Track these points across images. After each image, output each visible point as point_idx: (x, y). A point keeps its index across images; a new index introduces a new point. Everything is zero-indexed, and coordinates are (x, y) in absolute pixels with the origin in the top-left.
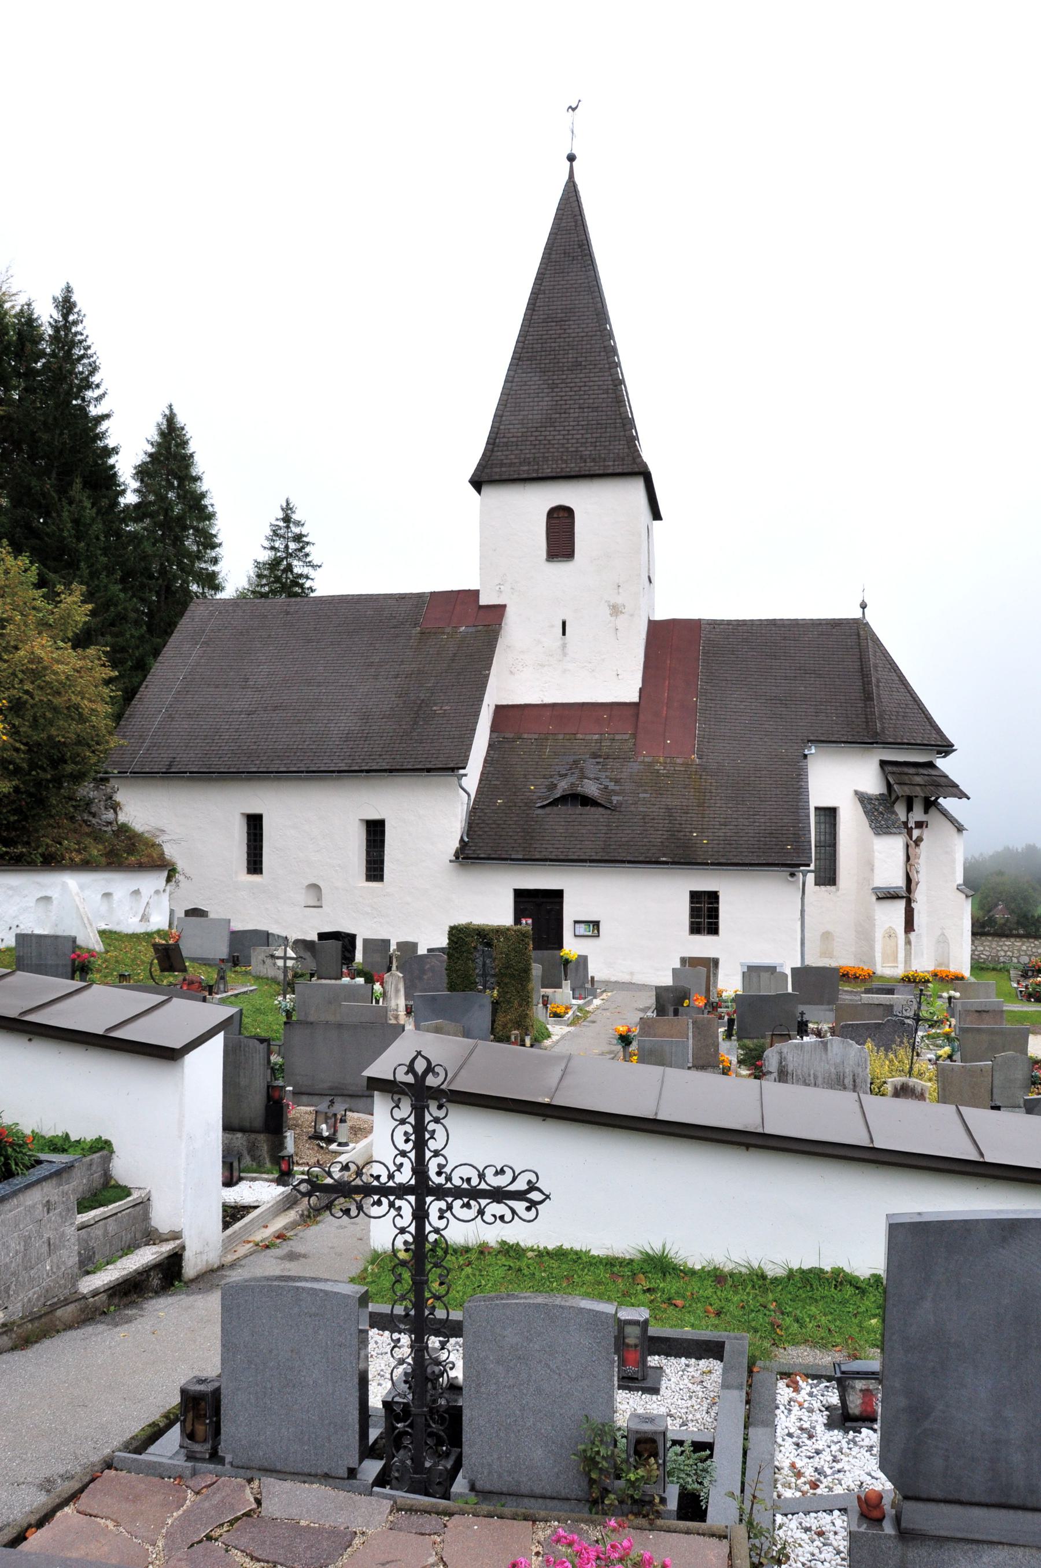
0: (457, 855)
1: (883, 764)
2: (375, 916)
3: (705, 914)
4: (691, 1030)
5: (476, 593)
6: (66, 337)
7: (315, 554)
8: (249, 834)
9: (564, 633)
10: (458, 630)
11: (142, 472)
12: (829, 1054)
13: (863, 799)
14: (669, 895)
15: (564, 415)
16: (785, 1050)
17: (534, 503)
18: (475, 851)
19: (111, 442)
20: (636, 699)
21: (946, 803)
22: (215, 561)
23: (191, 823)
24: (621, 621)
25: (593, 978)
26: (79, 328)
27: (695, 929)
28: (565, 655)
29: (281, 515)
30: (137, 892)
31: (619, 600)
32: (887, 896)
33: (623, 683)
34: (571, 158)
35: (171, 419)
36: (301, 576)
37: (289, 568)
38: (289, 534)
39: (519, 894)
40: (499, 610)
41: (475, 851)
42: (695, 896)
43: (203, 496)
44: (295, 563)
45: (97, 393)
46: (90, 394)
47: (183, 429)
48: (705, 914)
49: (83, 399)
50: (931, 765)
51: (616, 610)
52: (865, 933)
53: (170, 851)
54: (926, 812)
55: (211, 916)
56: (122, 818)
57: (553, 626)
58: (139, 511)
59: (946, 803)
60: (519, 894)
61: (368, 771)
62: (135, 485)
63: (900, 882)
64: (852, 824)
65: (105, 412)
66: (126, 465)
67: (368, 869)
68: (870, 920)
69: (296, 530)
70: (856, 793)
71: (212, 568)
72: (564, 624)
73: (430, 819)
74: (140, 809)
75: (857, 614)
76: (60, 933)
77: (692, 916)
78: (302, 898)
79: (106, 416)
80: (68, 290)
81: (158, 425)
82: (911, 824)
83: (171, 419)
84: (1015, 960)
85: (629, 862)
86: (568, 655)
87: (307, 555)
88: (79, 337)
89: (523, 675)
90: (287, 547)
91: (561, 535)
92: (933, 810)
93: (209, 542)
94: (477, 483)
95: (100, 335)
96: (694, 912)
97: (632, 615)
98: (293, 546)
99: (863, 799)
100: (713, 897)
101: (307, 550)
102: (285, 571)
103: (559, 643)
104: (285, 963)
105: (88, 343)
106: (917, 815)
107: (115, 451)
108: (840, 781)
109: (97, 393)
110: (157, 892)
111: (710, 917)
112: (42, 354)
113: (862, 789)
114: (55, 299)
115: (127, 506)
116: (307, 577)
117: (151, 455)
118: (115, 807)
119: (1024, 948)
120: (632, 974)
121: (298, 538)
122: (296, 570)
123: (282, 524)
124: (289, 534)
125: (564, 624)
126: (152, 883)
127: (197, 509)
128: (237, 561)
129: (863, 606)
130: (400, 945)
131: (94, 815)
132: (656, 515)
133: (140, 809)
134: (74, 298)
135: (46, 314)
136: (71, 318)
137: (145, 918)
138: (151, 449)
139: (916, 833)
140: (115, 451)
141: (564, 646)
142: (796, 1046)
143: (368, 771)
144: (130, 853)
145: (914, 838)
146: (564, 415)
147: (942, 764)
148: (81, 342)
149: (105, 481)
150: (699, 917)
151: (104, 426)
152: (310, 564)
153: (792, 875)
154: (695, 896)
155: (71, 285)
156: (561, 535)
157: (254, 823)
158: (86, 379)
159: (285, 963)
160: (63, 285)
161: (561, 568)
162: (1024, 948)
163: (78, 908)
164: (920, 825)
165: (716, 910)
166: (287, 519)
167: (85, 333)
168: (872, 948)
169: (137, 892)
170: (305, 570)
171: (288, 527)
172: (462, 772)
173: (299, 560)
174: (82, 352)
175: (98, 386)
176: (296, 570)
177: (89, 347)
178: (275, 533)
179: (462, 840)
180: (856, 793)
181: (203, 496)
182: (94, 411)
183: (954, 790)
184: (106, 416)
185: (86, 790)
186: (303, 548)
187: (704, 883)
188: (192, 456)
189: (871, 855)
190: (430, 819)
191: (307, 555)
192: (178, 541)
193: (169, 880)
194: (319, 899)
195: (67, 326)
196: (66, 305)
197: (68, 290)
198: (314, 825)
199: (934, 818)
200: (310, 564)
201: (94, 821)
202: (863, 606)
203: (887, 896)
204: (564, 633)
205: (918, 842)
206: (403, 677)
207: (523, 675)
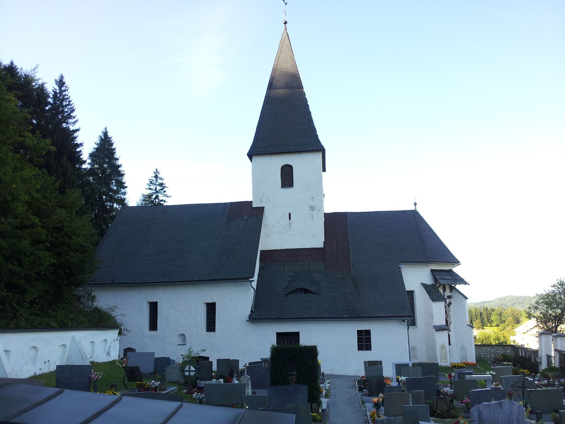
0: (250, 317)
1: (432, 271)
2: (218, 348)
3: (364, 340)
4: (411, 399)
5: (251, 203)
6: (61, 97)
7: (168, 191)
8: (150, 311)
9: (290, 219)
10: (245, 217)
11: (92, 155)
12: (504, 409)
13: (424, 285)
14: (348, 332)
15: (286, 126)
16: (481, 408)
17: (275, 163)
18: (258, 316)
19: (78, 141)
20: (322, 246)
21: (458, 287)
22: (125, 193)
23: (129, 306)
24: (315, 213)
25: (323, 373)
26: (66, 93)
27: (360, 348)
28: (291, 228)
29: (154, 175)
30: (105, 340)
31: (313, 204)
32: (439, 329)
33: (315, 238)
34: (286, 23)
35: (105, 134)
36: (162, 201)
37: (157, 197)
38: (157, 183)
39: (279, 335)
40: (261, 210)
41: (258, 316)
42: (359, 332)
43: (119, 166)
44: (159, 195)
45: (74, 120)
46: (70, 121)
47: (111, 138)
48: (364, 340)
49: (67, 123)
50: (451, 271)
51: (312, 208)
52: (431, 346)
53: (119, 319)
54: (451, 292)
55: (137, 351)
56: (95, 304)
57: (285, 216)
58: (91, 172)
59: (458, 287)
60: (279, 335)
61: (208, 280)
62: (89, 161)
63: (444, 323)
64: (421, 299)
65: (78, 128)
66: (86, 152)
67: (208, 326)
68: (434, 341)
69: (160, 181)
70: (422, 284)
71: (123, 197)
72: (290, 214)
73: (236, 301)
74: (104, 300)
75: (413, 208)
76: (69, 364)
77: (358, 342)
78: (179, 341)
79: (78, 130)
80: (62, 77)
81: (101, 137)
82: (446, 297)
83: (105, 134)
84: (488, 356)
85: (329, 318)
86: (290, 230)
87: (165, 192)
88: (66, 97)
89: (276, 236)
90: (156, 189)
91: (287, 177)
92: (454, 290)
93: (121, 185)
94: (251, 155)
95: (75, 95)
96: (360, 340)
97: (319, 210)
98: (158, 188)
99: (424, 285)
100: (368, 332)
101: (165, 189)
102: (155, 199)
103: (288, 222)
104: (190, 373)
105: (70, 99)
106: (448, 293)
107: (81, 145)
108: (415, 278)
109: (74, 120)
110: (114, 340)
111: (366, 342)
112: (49, 103)
113: (424, 282)
114: (56, 81)
115: (85, 169)
116: (165, 201)
117: (96, 149)
118: (93, 299)
119: (492, 351)
120: (333, 370)
121: (161, 185)
122: (160, 198)
123: (154, 179)
124: (157, 183)
125: (290, 214)
126: (112, 335)
127: (116, 172)
128: (134, 196)
129: (415, 204)
130: (220, 362)
131: (82, 303)
132: (324, 170)
133: (104, 300)
134: (64, 80)
135: (51, 87)
136: (63, 89)
137: (108, 354)
138: (96, 146)
139: (448, 301)
140: (81, 145)
141: (290, 224)
142: (486, 406)
143: (208, 280)
144: (102, 321)
145: (447, 303)
146: (286, 126)
147: (456, 270)
148: (67, 99)
149: (76, 159)
150: (362, 342)
151: (75, 135)
152: (166, 196)
153: (404, 321)
154: (359, 332)
155: (63, 74)
156: (287, 177)
157: (153, 307)
158: (69, 114)
159: (190, 373)
160: (60, 75)
161: (287, 191)
162: (492, 351)
163: (80, 350)
164: (449, 297)
165: (370, 339)
166: (156, 177)
167: (69, 95)
168: (435, 354)
169: (105, 340)
170: (164, 198)
171: (157, 180)
172: (251, 279)
173: (161, 194)
174: (68, 103)
175: (74, 117)
176: (160, 198)
177: (70, 101)
178: (151, 182)
179: (252, 311)
180: (422, 284)
181: (119, 166)
182: (72, 128)
183: (462, 281)
184: (78, 130)
185: (80, 291)
186: (163, 189)
187: (364, 326)
188: (115, 149)
189: (429, 311)
190: (236, 301)
191: (165, 192)
192: (108, 185)
193: (120, 334)
194: (184, 341)
195: (61, 92)
196: (61, 83)
197: (62, 77)
198: (182, 308)
199: (454, 294)
200: (166, 196)
201: (82, 306)
202: (415, 204)
203: (439, 329)
204: (290, 219)
205: (450, 304)
206: (216, 240)
207: (276, 236)
